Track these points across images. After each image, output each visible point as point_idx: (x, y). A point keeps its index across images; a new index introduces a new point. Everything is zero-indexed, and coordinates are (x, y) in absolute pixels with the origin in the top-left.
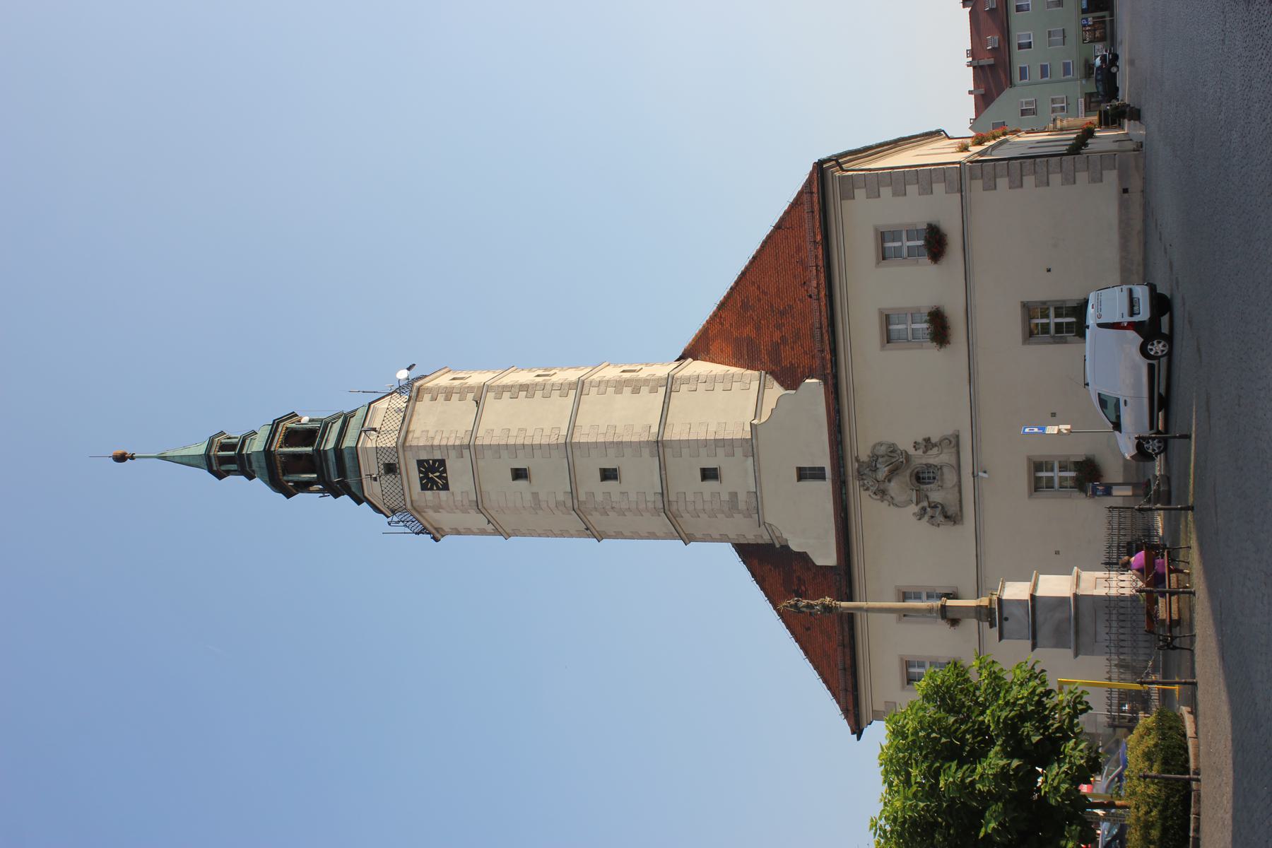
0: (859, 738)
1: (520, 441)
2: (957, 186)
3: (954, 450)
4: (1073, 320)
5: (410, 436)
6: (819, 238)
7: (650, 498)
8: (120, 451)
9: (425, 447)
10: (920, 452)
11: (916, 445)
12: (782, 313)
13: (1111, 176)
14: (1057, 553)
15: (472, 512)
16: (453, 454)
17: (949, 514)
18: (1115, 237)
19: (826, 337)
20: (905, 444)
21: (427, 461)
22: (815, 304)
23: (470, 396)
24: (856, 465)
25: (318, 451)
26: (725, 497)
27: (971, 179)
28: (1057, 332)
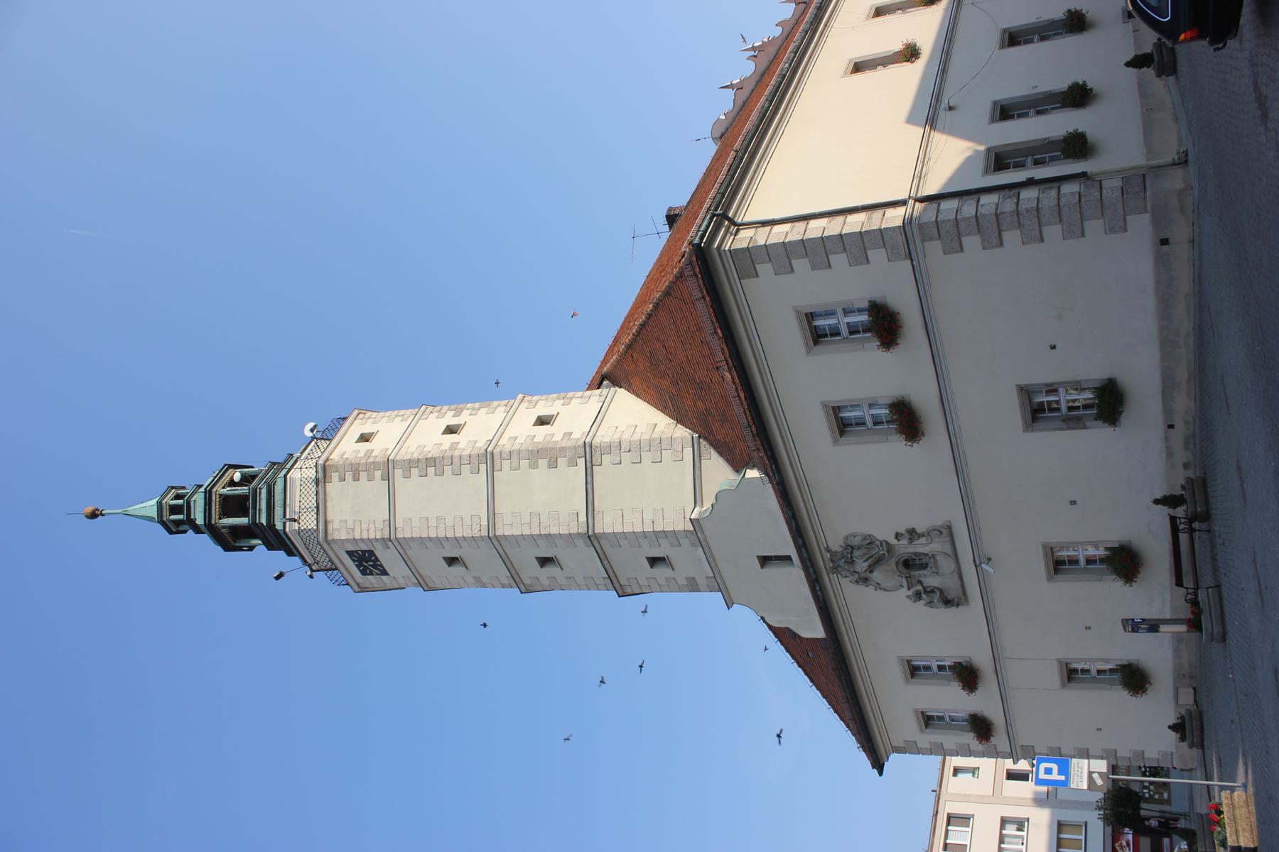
0: (881, 773)
2: (902, 250)
3: (948, 539)
9: (347, 540)
10: (904, 542)
13: (1141, 224)
14: (1088, 628)
17: (950, 598)
18: (1150, 302)
20: (884, 533)
23: (378, 474)
25: (254, 523)
27: (923, 240)
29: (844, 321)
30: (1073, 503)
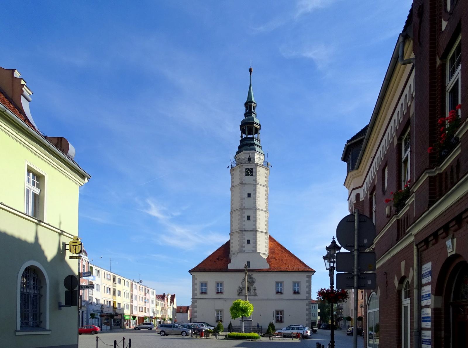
1: (257, 196)
3: (253, 295)
4: (279, 319)
5: (259, 167)
6: (300, 270)
7: (244, 227)
8: (252, 70)
10: (253, 288)
11: (255, 287)
12: (282, 260)
15: (240, 181)
16: (255, 178)
19: (279, 270)
20: (255, 285)
21: (253, 171)
22: (286, 268)
24: (251, 274)
26: (244, 245)
27: (309, 301)
28: (282, 315)
29: (279, 287)
30: (261, 315)
